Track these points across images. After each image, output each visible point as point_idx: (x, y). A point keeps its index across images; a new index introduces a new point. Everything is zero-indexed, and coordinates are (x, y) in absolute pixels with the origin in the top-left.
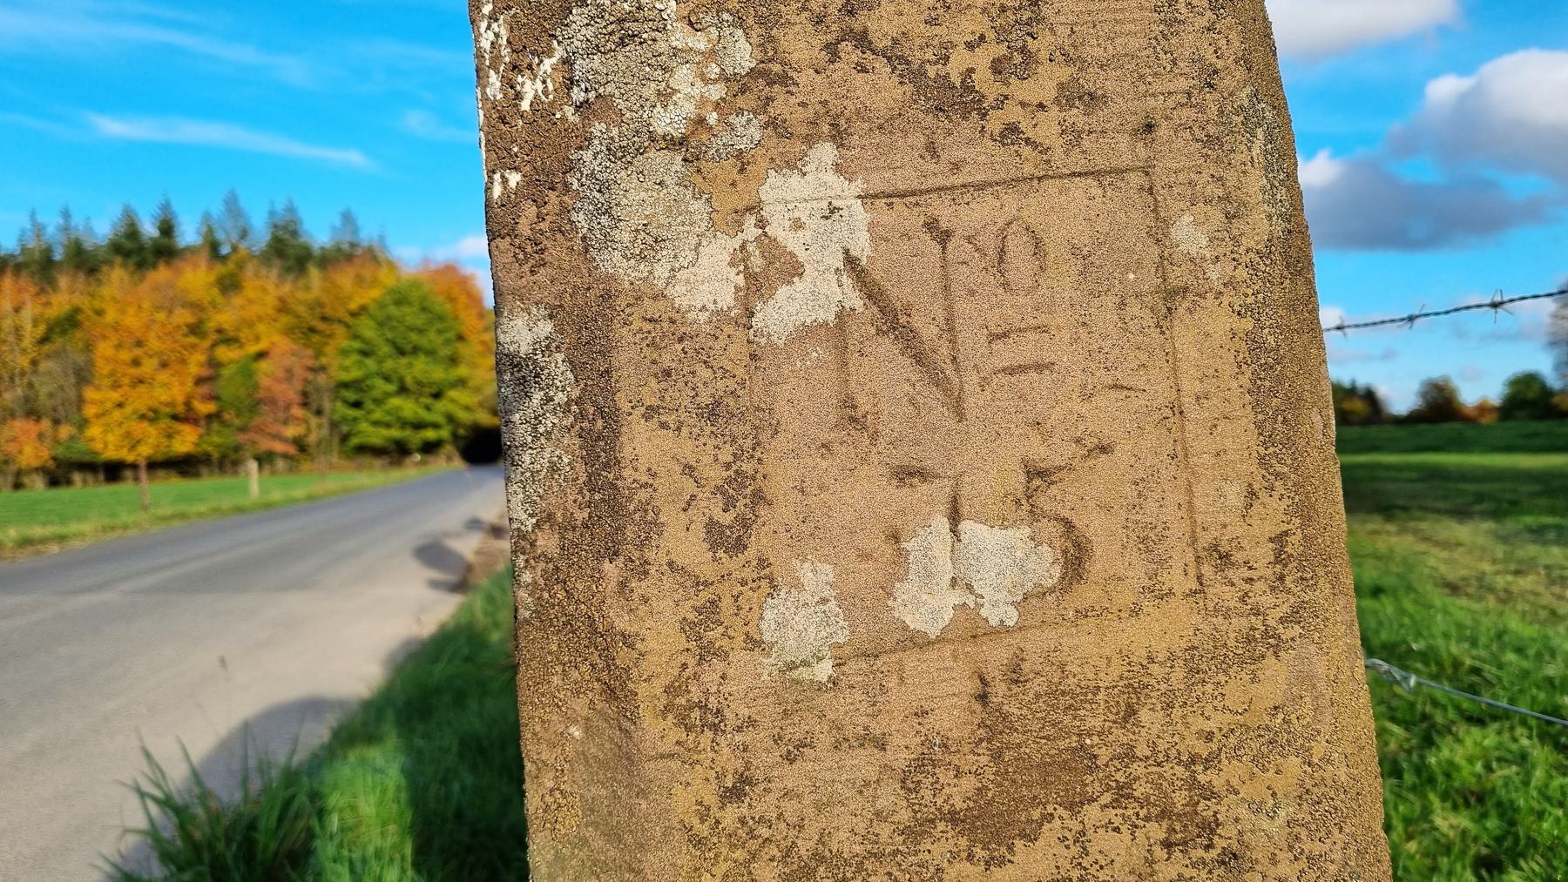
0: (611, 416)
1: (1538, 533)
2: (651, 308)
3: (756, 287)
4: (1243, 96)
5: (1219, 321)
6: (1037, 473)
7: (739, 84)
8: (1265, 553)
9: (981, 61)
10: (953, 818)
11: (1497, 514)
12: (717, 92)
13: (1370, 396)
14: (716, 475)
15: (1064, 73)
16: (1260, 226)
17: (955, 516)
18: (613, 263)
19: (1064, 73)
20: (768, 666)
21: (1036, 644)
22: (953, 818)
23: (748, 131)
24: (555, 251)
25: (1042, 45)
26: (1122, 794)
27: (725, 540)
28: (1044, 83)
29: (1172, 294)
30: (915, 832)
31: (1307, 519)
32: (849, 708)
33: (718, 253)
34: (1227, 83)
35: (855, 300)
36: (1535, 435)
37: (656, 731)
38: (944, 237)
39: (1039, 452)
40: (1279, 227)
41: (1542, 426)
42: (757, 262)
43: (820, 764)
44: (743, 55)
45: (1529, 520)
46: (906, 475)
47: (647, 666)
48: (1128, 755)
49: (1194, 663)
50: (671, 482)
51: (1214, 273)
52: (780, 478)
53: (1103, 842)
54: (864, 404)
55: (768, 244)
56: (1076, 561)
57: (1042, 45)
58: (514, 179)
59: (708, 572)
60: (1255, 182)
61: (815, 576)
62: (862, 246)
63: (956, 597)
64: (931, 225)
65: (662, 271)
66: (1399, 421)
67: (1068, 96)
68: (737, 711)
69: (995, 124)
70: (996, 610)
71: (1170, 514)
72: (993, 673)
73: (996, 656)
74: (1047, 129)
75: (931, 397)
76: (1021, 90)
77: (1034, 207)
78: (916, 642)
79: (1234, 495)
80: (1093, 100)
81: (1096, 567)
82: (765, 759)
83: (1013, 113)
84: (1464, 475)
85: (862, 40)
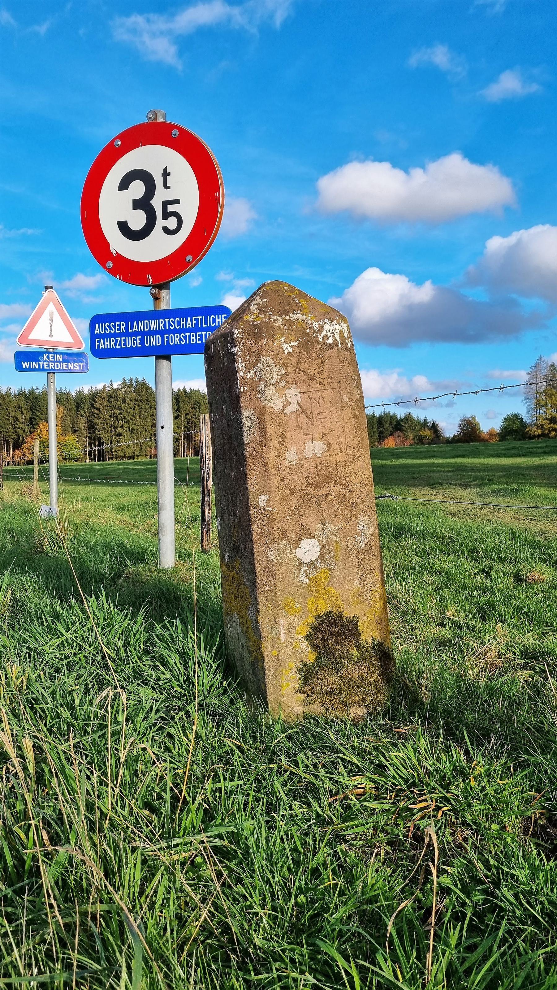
0: (265, 425)
1: (496, 493)
2: (271, 409)
3: (285, 406)
4: (353, 377)
5: (350, 411)
6: (324, 434)
7: (283, 376)
8: (356, 446)
9: (316, 372)
10: (312, 484)
11: (481, 486)
12: (279, 377)
13: (434, 427)
14: (280, 434)
15: (328, 373)
16: (356, 396)
17: (312, 440)
18: (265, 403)
19: (328, 373)
20: (287, 462)
21: (324, 459)
22: (312, 484)
23: (284, 383)
24: (254, 400)
25: (324, 369)
26: (336, 481)
27: (281, 443)
28: (325, 375)
29: (343, 407)
30: (307, 486)
31: (362, 441)
32: (298, 468)
33: (280, 401)
34: (351, 375)
35: (299, 408)
36: (513, 448)
37: (272, 471)
38: (311, 399)
39: (325, 431)
40: (358, 396)
41: (517, 444)
42: (285, 403)
43: (294, 476)
44: (283, 372)
45: (493, 487)
46: (305, 434)
47: (271, 462)
48: (337, 476)
49: (346, 462)
50: (274, 435)
51: (349, 404)
52: (288, 436)
53: (332, 488)
54: (300, 424)
55: (286, 400)
56: (329, 447)
57: (324, 369)
58: (246, 388)
59: (279, 448)
60: (355, 390)
61: (293, 449)
62: (300, 400)
63: (313, 452)
64: (309, 397)
65: (272, 404)
66: (449, 442)
67: (329, 377)
68: (283, 469)
69: (318, 382)
70: (318, 454)
71: (343, 440)
72: (318, 463)
73: (318, 461)
74: (325, 382)
75: (309, 422)
76: (321, 376)
77: (323, 394)
78: (307, 459)
79: (352, 437)
80: (332, 378)
81: (332, 448)
82: (287, 476)
83: (320, 380)
84: (473, 469)
85: (299, 369)
